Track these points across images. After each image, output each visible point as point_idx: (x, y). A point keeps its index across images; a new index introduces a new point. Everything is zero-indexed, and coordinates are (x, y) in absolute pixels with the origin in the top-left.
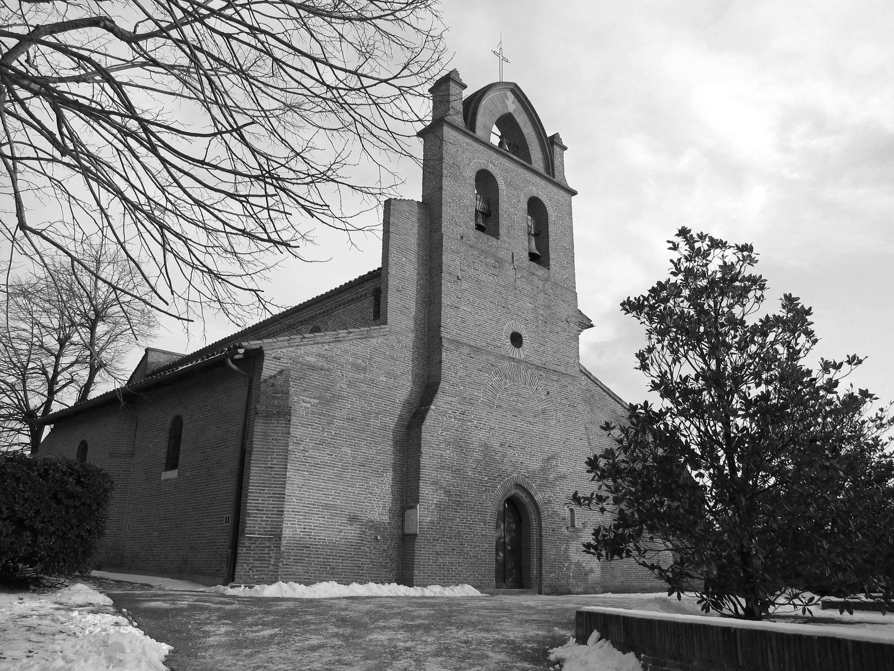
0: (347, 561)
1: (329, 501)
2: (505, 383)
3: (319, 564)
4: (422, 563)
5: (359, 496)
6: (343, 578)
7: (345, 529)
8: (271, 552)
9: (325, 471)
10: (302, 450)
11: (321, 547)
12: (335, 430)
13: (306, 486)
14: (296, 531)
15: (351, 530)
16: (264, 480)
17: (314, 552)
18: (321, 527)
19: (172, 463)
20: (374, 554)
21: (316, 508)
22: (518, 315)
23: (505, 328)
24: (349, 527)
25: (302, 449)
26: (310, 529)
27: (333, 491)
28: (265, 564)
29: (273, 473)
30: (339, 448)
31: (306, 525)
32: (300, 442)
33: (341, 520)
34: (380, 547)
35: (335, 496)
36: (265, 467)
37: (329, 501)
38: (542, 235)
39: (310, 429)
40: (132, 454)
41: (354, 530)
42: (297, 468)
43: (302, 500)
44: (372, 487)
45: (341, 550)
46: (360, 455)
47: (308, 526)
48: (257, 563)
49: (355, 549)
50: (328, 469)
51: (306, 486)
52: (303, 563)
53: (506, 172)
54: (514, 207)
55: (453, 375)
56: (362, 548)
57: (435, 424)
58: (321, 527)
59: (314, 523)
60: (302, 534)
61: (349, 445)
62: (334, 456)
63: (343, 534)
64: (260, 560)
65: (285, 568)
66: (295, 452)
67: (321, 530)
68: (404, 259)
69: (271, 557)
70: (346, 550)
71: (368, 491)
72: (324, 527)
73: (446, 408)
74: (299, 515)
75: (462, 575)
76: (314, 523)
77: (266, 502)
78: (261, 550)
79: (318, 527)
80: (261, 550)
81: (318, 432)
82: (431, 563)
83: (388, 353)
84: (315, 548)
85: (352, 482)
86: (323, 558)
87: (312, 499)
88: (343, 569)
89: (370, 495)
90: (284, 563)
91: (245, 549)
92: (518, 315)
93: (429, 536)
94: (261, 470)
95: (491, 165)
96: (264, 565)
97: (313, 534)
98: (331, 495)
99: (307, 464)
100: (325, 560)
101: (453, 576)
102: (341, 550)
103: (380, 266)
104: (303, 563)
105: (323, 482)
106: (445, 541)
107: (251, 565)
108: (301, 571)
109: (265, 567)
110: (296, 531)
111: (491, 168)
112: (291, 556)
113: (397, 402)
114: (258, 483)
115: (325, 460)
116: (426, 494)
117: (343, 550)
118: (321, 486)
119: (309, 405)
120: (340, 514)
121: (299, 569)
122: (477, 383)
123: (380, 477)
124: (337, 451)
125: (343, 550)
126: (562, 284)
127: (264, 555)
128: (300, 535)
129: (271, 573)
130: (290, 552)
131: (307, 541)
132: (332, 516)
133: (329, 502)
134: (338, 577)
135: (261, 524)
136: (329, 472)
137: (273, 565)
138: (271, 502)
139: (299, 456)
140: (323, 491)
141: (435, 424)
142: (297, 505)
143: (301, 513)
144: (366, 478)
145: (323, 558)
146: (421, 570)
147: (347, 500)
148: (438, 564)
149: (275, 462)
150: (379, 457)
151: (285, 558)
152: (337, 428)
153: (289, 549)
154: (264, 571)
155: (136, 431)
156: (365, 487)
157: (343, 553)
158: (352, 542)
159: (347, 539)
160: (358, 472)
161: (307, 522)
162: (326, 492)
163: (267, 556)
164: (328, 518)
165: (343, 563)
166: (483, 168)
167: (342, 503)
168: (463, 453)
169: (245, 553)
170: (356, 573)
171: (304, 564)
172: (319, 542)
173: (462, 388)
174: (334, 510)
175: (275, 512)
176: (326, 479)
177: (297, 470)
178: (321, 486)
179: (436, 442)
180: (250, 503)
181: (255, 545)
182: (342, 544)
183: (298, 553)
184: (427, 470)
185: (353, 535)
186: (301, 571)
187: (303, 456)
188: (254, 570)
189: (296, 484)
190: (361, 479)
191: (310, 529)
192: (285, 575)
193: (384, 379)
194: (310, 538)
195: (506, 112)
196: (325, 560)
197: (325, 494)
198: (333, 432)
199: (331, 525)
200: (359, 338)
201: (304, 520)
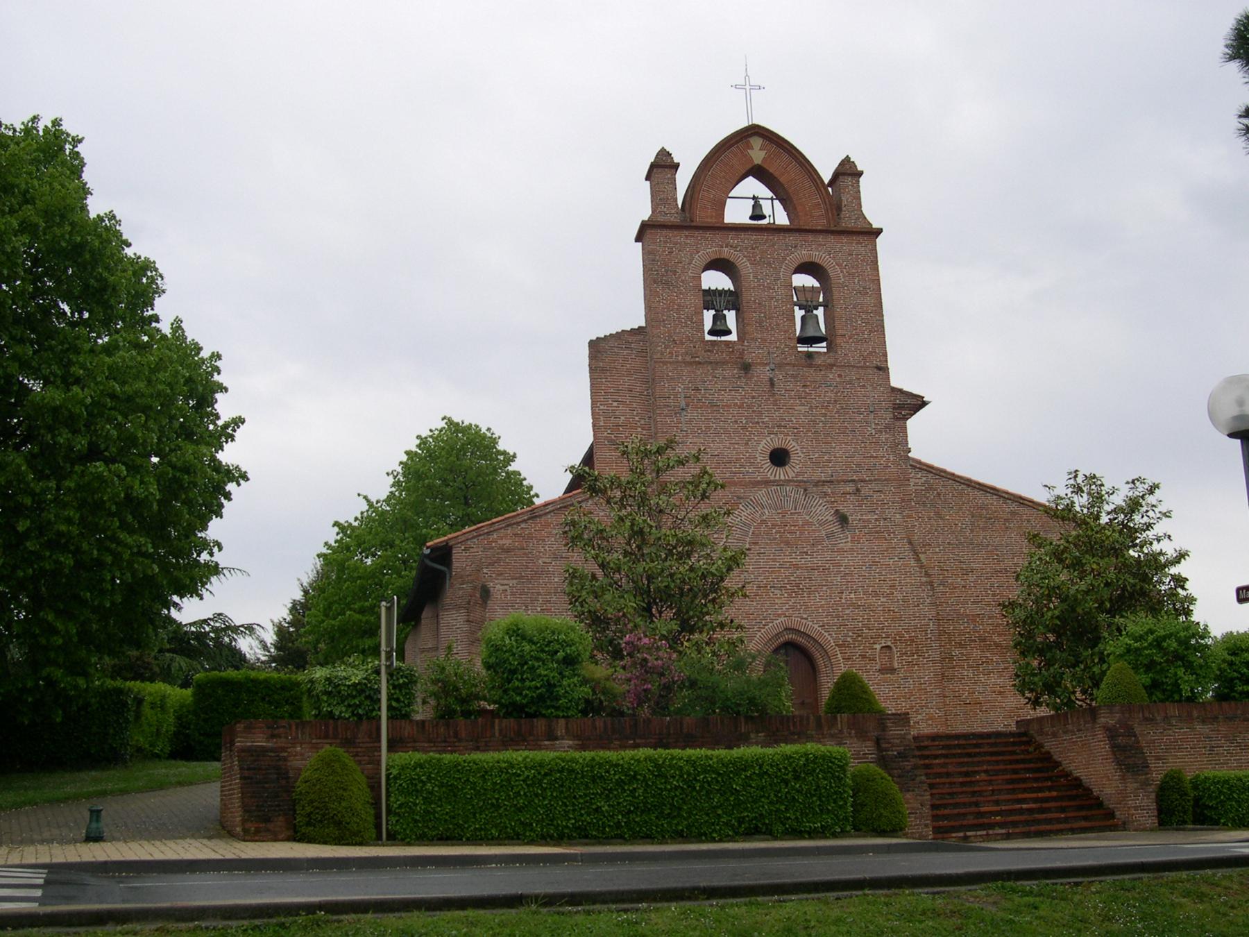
2: (763, 514)
23: (759, 448)
53: (753, 249)
92: (779, 426)
163: (867, 752)
200: (560, 508)
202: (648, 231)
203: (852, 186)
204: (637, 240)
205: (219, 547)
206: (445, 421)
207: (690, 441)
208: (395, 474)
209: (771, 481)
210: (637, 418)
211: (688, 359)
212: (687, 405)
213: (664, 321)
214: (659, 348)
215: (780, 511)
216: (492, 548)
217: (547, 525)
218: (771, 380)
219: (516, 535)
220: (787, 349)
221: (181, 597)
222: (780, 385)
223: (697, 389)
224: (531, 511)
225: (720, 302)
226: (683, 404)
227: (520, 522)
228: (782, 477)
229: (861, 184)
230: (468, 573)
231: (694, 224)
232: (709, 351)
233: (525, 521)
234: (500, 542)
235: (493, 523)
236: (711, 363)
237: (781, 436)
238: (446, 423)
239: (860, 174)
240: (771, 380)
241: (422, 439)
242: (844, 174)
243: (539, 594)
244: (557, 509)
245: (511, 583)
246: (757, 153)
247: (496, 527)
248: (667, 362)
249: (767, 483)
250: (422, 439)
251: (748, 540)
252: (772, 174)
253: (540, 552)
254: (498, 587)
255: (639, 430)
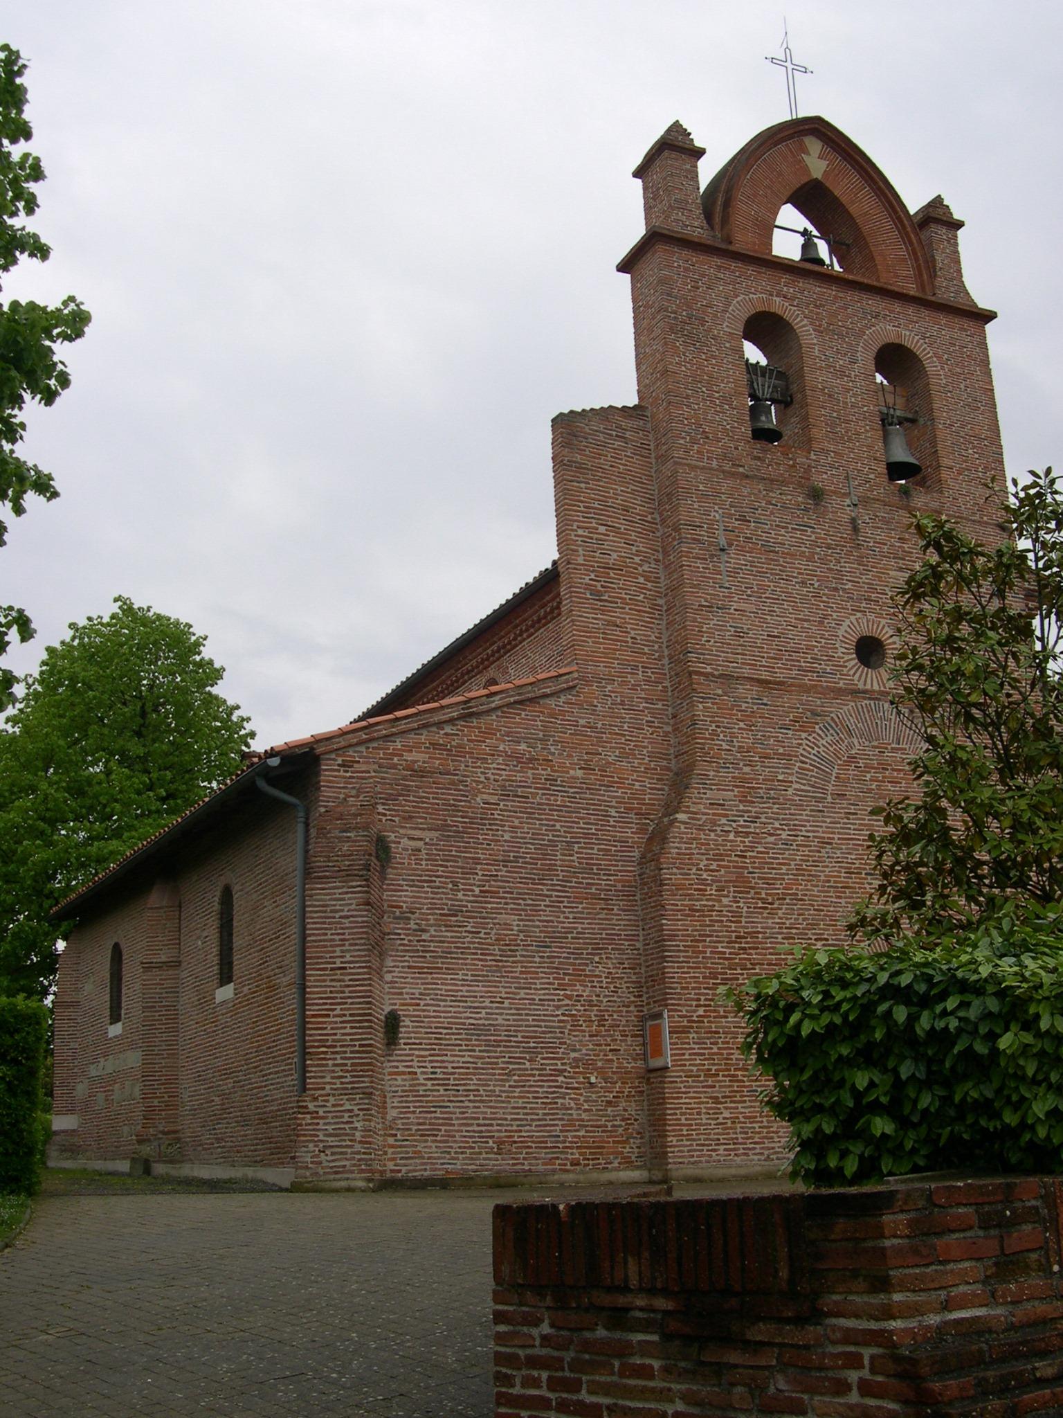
0: (528, 1128)
1: (481, 1019)
2: (851, 746)
3: (470, 1137)
4: (683, 1121)
5: (543, 1005)
6: (524, 1159)
7: (519, 1069)
8: (354, 1119)
9: (466, 964)
10: (415, 930)
11: (471, 1105)
12: (479, 886)
13: (429, 995)
14: (418, 1079)
15: (532, 1069)
16: (331, 992)
17: (458, 1115)
18: (468, 1068)
19: (226, 977)
20: (586, 1110)
21: (453, 1034)
22: (869, 600)
23: (840, 633)
24: (528, 1063)
25: (416, 927)
26: (444, 1073)
27: (488, 1000)
28: (345, 1140)
29: (347, 978)
30: (492, 919)
31: (435, 1067)
32: (409, 915)
33: (510, 1052)
34: (600, 1097)
35: (491, 1008)
36: (332, 969)
37: (481, 1019)
38: (921, 421)
39: (426, 889)
40: (177, 964)
41: (537, 1069)
42: (406, 964)
43: (423, 1022)
44: (571, 985)
45: (514, 1108)
46: (538, 927)
47: (440, 1067)
48: (332, 1141)
49: (543, 1103)
50: (472, 959)
51: (429, 995)
52: (436, 1136)
53: (816, 306)
54: (843, 374)
55: (725, 746)
56: (560, 1101)
57: (690, 848)
58: (468, 1068)
59: (453, 1062)
60: (429, 1083)
61: (512, 909)
62: (482, 935)
63: (516, 1078)
64: (336, 1135)
65: (401, 1146)
66: (399, 934)
67: (467, 1074)
68: (602, 529)
69: (356, 1129)
70: (525, 1108)
71: (562, 993)
72: (474, 1068)
73: (714, 814)
74: (419, 1049)
75: (776, 1140)
76: (453, 1062)
77: (339, 1031)
78: (337, 1117)
79: (462, 1068)
80: (337, 1117)
81: (444, 893)
82: (704, 1121)
83: (582, 722)
84: (459, 1107)
85: (526, 979)
86: (478, 1125)
87: (445, 1018)
88: (521, 1142)
89: (567, 1002)
90: (399, 1137)
91: (308, 1116)
92: (869, 600)
93: (695, 1069)
94: (324, 975)
95: (778, 299)
96: (344, 1144)
97: (452, 1082)
98: (483, 1008)
99: (428, 955)
100: (483, 1128)
101: (755, 1143)
102: (514, 1108)
103: (556, 556)
104: (436, 1136)
105: (463, 985)
106: (733, 1076)
107: (321, 1145)
108: (434, 1149)
109: (347, 1146)
110: (418, 1079)
111: (778, 305)
112: (412, 1124)
113: (614, 814)
114: (322, 998)
115: (464, 943)
116: (682, 988)
117: (518, 1108)
118: (460, 994)
119: (420, 844)
120: (506, 1041)
121: (431, 1147)
122: (780, 754)
123: (587, 965)
124: (488, 923)
125: (518, 1108)
126: (977, 518)
127: (342, 1126)
128: (426, 1085)
129: (357, 1157)
130: (408, 1118)
131: (442, 1096)
132: (489, 1046)
133: (480, 1022)
134: (513, 1158)
135: (333, 1071)
136: (474, 965)
137: (360, 1142)
138: (348, 1031)
139: (410, 941)
140: (466, 1002)
141: (690, 848)
142: (413, 1032)
143: (423, 1046)
144: (557, 968)
145: (478, 1125)
146: (683, 1135)
147: (519, 1015)
148: (721, 1120)
149: (348, 958)
150: (580, 926)
151: (399, 1129)
152: (483, 881)
153: (406, 1113)
154: (346, 1153)
155: (180, 919)
156: (556, 986)
157: (518, 1114)
158: (537, 1092)
159: (524, 1086)
160: (537, 959)
161: (437, 1061)
162: (472, 1002)
163: (347, 1126)
164: (480, 1051)
165: (520, 1131)
166: (746, 316)
167: (509, 1020)
168: (759, 899)
169: (310, 1124)
170: (551, 1147)
171: (439, 1138)
172: (466, 1096)
173: (747, 769)
174: (492, 1035)
175: (357, 1048)
176: (470, 978)
177: (409, 967)
178: (460, 994)
179: (696, 884)
180: (311, 1035)
181: (325, 1109)
182: (514, 1097)
183: (426, 1118)
184: (681, 941)
185: (537, 1078)
186: (434, 1149)
187: (418, 941)
188: (328, 1152)
189: (407, 994)
190: (545, 973)
191: (444, 1073)
192: (402, 1158)
193: (579, 773)
194: (446, 1090)
195: (804, 180)
196: (483, 1128)
197: (470, 1007)
198: (477, 890)
199: (488, 1063)
200: (515, 702)
201: (430, 1058)
202: (660, 247)
203: (949, 242)
204: (624, 267)
205: (21, 632)
206: (119, 603)
207: (735, 606)
208: (30, 681)
209: (859, 691)
210: (637, 559)
211: (727, 466)
212: (730, 545)
213: (688, 397)
214: (682, 442)
215: (875, 743)
216: (394, 767)
217: (491, 733)
218: (853, 521)
219: (434, 745)
220: (872, 476)
221: (199, 653)
222: (867, 531)
223: (743, 519)
224: (465, 702)
225: (763, 385)
226: (723, 542)
227: (445, 722)
228: (876, 687)
229: (960, 241)
230: (353, 810)
231: (731, 248)
232: (759, 459)
233: (451, 721)
234: (409, 757)
235: (397, 719)
236: (764, 479)
237: (872, 617)
238: (120, 608)
239: (959, 225)
240: (853, 521)
241: (77, 630)
242: (938, 221)
243: (477, 861)
244: (509, 705)
245: (428, 835)
246: (816, 163)
247: (403, 726)
248: (697, 467)
249: (856, 693)
250: (77, 630)
251: (830, 788)
252: (836, 198)
253: (478, 782)
254: (405, 841)
255: (641, 580)
